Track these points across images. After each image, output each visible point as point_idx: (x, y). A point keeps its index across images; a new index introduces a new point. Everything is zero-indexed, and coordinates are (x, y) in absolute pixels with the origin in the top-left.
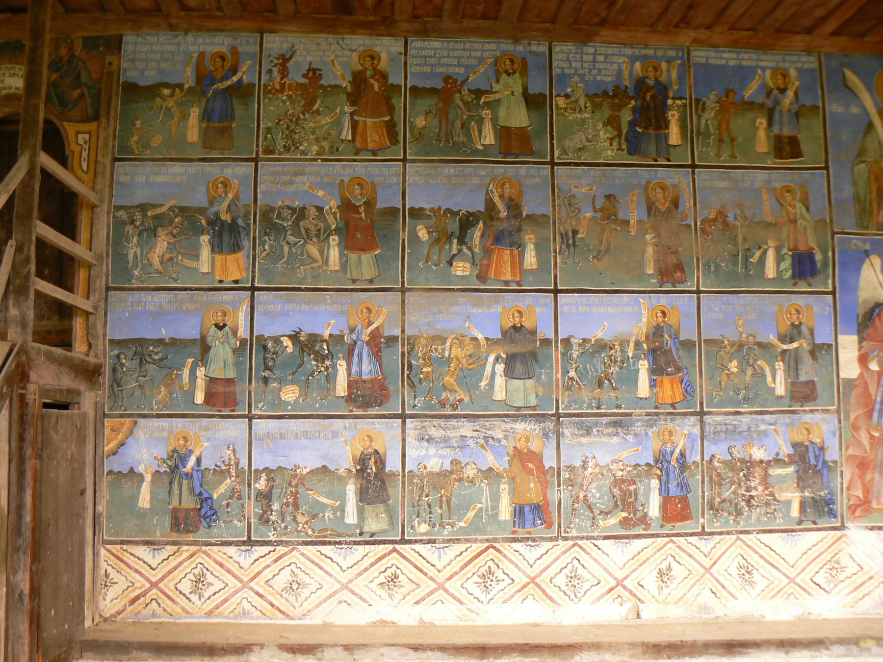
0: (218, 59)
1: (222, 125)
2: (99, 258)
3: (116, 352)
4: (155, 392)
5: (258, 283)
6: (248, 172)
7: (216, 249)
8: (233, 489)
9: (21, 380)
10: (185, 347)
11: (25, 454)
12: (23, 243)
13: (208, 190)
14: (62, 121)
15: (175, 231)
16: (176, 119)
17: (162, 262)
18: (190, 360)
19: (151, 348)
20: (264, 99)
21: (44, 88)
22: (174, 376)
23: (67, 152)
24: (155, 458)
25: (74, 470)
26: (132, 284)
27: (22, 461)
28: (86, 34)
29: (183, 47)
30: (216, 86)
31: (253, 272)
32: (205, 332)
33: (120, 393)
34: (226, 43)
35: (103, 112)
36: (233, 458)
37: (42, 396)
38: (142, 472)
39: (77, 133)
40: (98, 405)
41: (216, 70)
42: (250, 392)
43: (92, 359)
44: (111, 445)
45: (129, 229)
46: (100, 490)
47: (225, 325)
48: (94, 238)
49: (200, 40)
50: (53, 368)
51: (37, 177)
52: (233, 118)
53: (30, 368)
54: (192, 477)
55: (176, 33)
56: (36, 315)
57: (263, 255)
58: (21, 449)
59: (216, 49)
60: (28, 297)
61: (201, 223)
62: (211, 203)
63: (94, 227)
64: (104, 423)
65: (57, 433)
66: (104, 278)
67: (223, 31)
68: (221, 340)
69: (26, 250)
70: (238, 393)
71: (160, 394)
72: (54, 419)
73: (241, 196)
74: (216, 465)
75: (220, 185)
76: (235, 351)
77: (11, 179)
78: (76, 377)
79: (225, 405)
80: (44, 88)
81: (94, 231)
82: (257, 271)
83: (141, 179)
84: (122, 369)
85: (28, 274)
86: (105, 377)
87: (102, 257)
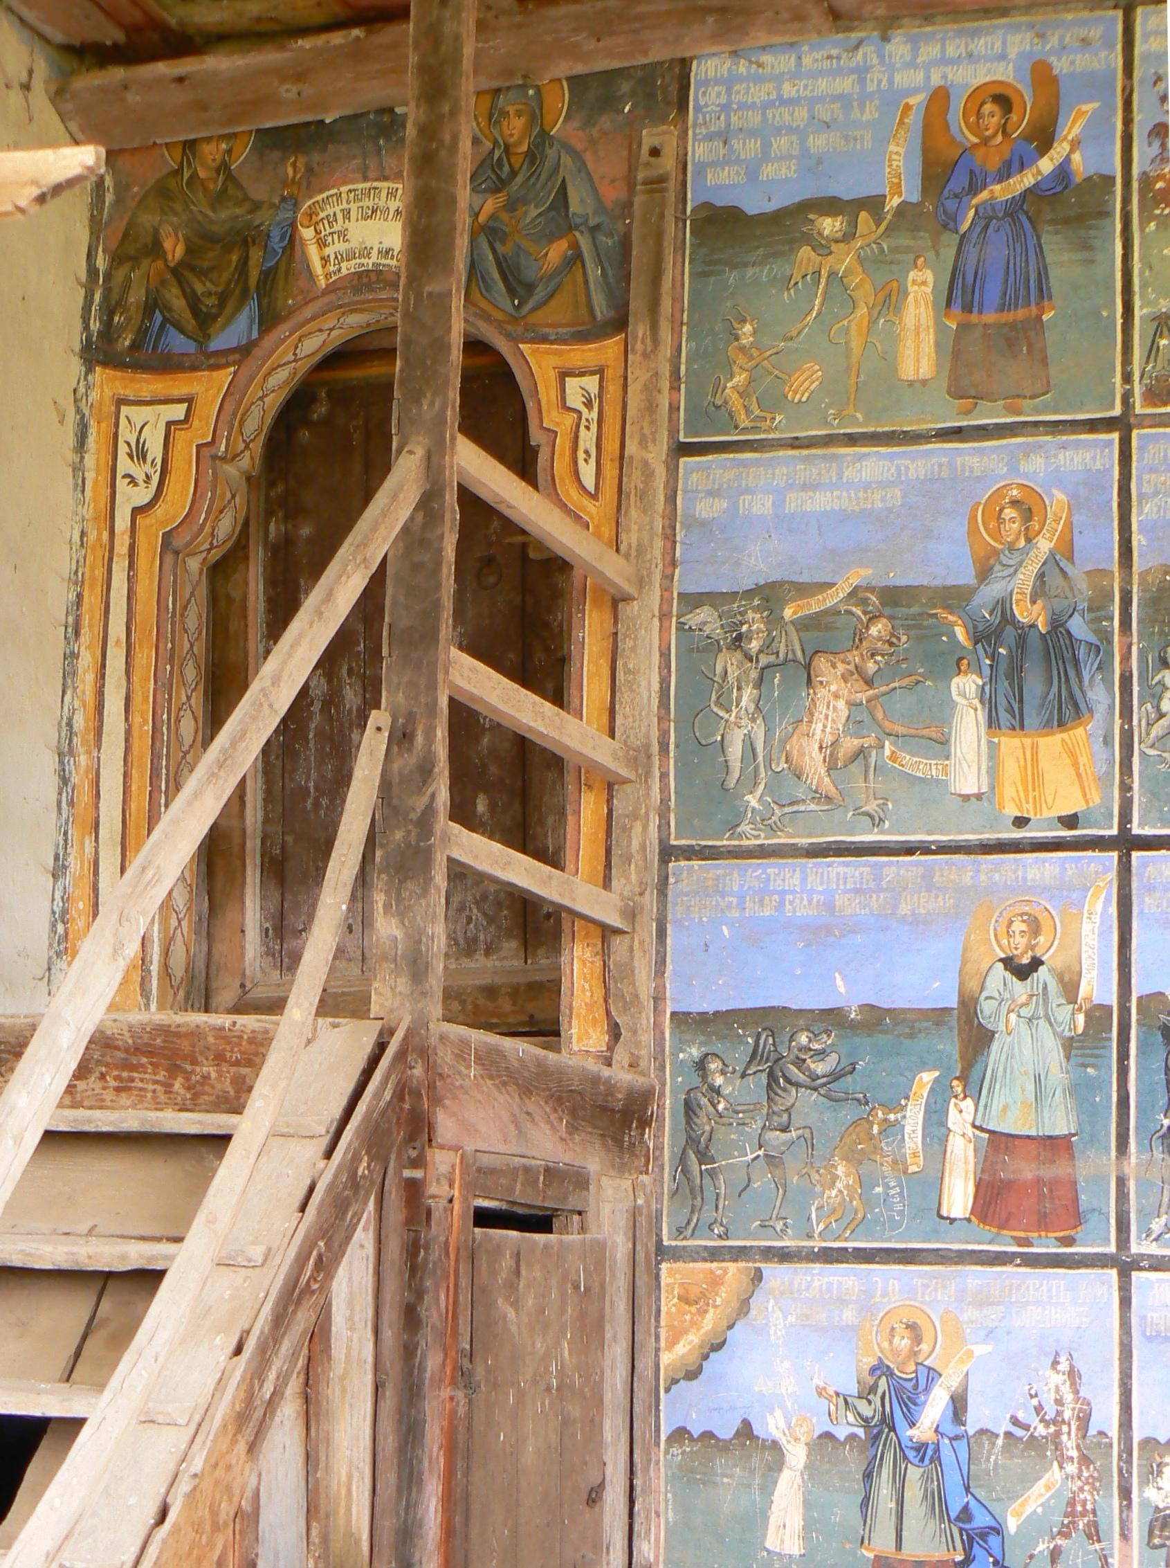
0: (988, 107)
1: (1009, 317)
2: (639, 758)
3: (695, 1052)
4: (815, 1177)
5: (1141, 825)
6: (1098, 466)
7: (1004, 716)
8: (1072, 1503)
9: (411, 1138)
10: (911, 1036)
11: (422, 1368)
12: (411, 717)
13: (973, 530)
14: (515, 340)
15: (871, 667)
16: (862, 311)
17: (831, 767)
18: (928, 1077)
19: (803, 1039)
20: (1143, 224)
21: (462, 243)
22: (875, 1129)
23: (536, 437)
24: (820, 1392)
25: (566, 1422)
26: (740, 837)
27: (412, 1392)
28: (579, 69)
29: (877, 79)
30: (984, 195)
31: (1126, 788)
32: (973, 985)
33: (707, 1180)
34: (1013, 53)
35: (637, 304)
36: (1069, 1397)
37: (470, 1188)
38: (777, 1435)
39: (564, 375)
40: (642, 1220)
41: (986, 141)
42: (1121, 1182)
43: (621, 1075)
44: (681, 1349)
45: (728, 663)
46: (647, 1491)
47: (1036, 963)
48: (624, 697)
49: (930, 51)
50: (506, 1101)
51: (448, 516)
52: (1043, 293)
53: (436, 1101)
54: (937, 1458)
55: (855, 36)
56: (452, 938)
57: (1157, 730)
58: (409, 1351)
59: (980, 75)
60: (428, 880)
61: (952, 635)
62: (984, 573)
63: (620, 663)
64: (657, 1277)
65: (516, 1305)
66: (655, 821)
67: (1004, 12)
68: (1024, 1012)
69: (419, 739)
70: (1082, 1184)
71: (832, 1185)
72: (507, 1262)
73: (1079, 542)
74: (1015, 1421)
75: (1009, 513)
76: (1069, 1045)
77: (374, 528)
78: (573, 1129)
79: (1043, 1223)
80: (462, 243)
81: (620, 676)
82: (1136, 786)
83: (762, 505)
84: (714, 1106)
85: (429, 811)
86: (661, 1128)
87: (649, 757)
